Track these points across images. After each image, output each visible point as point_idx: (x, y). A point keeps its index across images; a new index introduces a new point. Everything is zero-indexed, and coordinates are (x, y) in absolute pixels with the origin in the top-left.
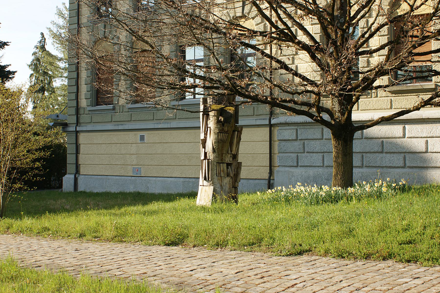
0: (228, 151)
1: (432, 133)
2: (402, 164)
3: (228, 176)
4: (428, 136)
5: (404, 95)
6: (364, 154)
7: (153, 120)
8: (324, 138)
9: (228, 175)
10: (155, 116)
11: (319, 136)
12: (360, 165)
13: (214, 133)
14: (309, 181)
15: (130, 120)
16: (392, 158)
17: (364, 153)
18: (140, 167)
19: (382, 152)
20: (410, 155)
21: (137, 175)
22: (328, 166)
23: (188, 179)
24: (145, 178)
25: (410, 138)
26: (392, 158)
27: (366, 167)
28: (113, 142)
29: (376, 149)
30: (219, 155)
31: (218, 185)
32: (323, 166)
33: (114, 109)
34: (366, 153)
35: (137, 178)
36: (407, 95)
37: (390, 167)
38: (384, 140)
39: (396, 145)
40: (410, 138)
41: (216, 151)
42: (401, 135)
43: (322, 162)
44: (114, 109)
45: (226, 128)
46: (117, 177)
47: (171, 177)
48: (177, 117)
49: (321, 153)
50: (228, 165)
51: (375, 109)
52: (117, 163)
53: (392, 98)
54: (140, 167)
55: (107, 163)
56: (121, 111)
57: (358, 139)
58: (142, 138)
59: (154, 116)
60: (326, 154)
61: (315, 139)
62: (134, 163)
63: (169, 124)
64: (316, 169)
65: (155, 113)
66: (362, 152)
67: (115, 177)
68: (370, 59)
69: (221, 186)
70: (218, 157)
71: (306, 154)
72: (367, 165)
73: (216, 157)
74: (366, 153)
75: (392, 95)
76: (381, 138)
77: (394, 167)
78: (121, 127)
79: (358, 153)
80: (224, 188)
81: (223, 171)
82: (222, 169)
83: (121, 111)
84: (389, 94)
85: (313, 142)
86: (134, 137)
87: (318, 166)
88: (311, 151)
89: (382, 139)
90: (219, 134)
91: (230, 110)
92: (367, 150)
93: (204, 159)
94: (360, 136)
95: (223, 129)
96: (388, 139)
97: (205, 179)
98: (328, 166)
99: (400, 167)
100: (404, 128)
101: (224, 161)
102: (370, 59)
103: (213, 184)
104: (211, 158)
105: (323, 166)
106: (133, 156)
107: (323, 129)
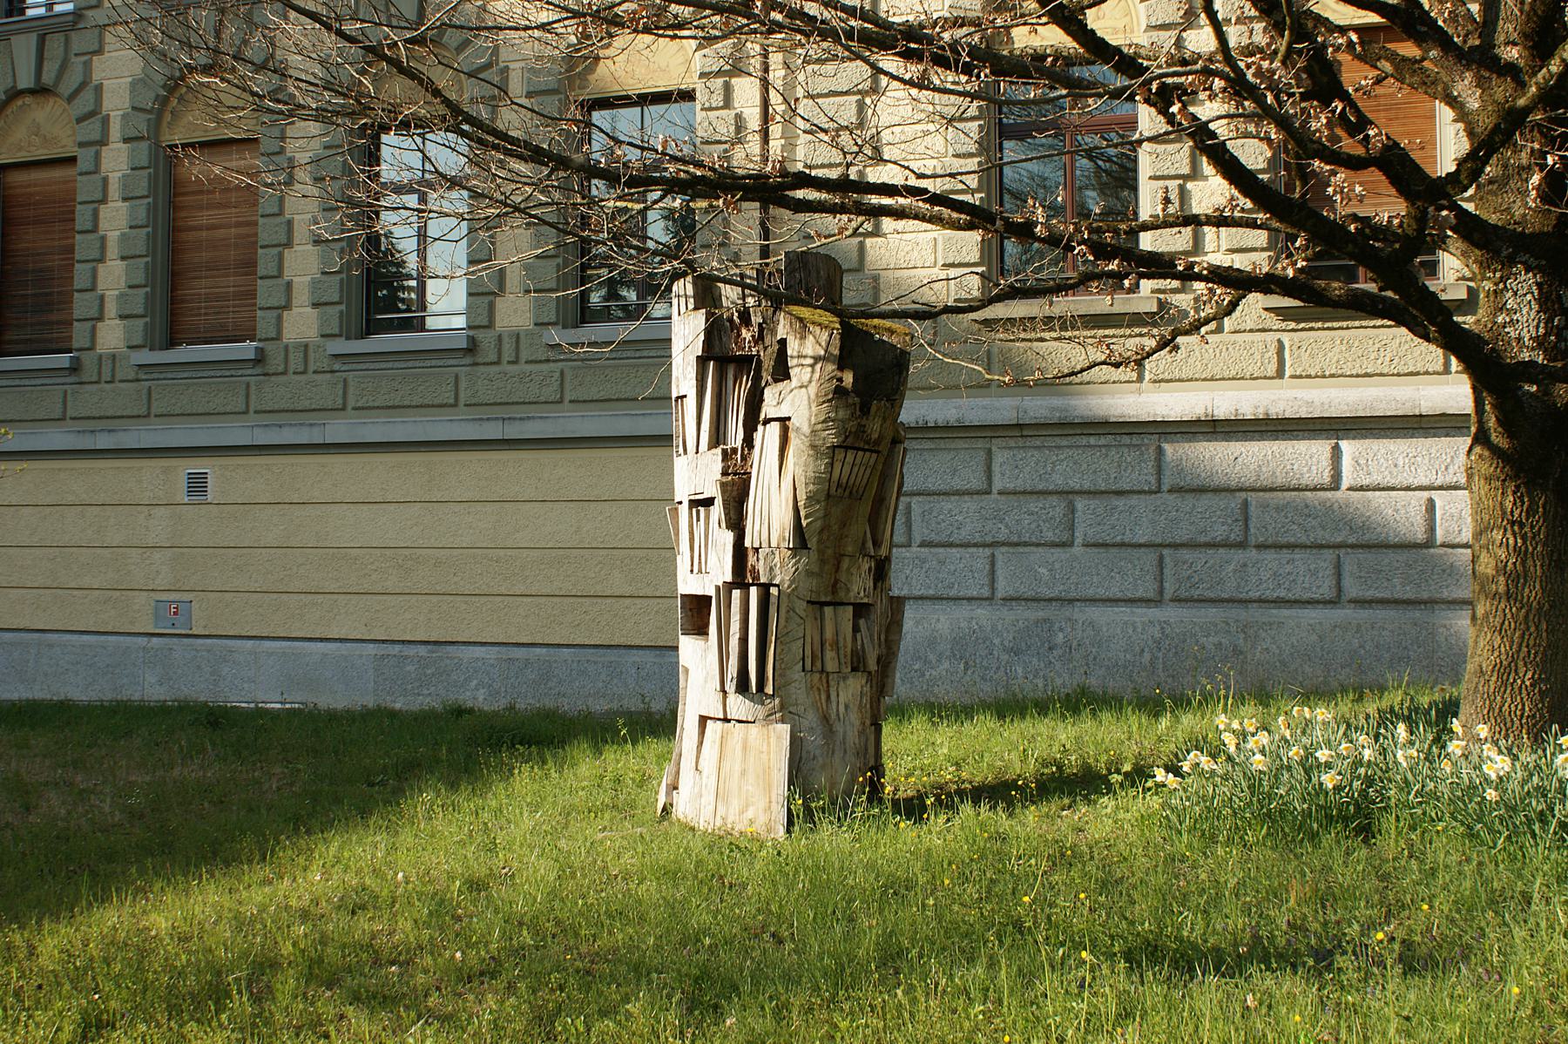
0: (864, 543)
1: (1451, 470)
2: (1326, 589)
3: (854, 669)
4: (1438, 483)
5: (1335, 324)
6: (1166, 552)
7: (246, 412)
8: (998, 484)
9: (858, 665)
10: (253, 397)
11: (976, 483)
12: (1151, 595)
13: (813, 447)
14: (932, 657)
15: (143, 411)
16: (1289, 568)
17: (1169, 546)
18: (186, 597)
19: (1242, 545)
20: (1362, 555)
21: (174, 626)
22: (1012, 599)
23: (398, 647)
24: (209, 641)
25: (1361, 489)
26: (1289, 568)
27: (1177, 600)
28: (70, 499)
29: (1219, 532)
30: (822, 561)
31: (811, 719)
32: (990, 599)
33: (75, 368)
34: (1175, 546)
35: (175, 640)
36: (1345, 324)
37: (1279, 602)
38: (1252, 496)
39: (1307, 511)
40: (1361, 489)
41: (813, 543)
42: (1326, 478)
43: (986, 581)
44: (75, 368)
45: (877, 427)
46: (85, 637)
47: (321, 640)
48: (351, 403)
49: (984, 545)
50: (861, 610)
51: (1212, 379)
52: (86, 581)
53: (1286, 339)
54: (186, 597)
55: (39, 582)
56: (106, 375)
57: (1144, 492)
58: (197, 484)
59: (247, 396)
60: (1004, 549)
61: (958, 493)
62: (160, 582)
63: (316, 430)
64: (962, 612)
65: (253, 388)
66: (1160, 545)
67: (75, 637)
68: (1189, 185)
69: (825, 719)
70: (819, 575)
71: (914, 549)
72: (1184, 595)
73: (809, 573)
74: (1175, 546)
75: (1283, 325)
76: (1241, 490)
77: (1296, 602)
78: (104, 442)
79: (1141, 546)
80: (839, 728)
81: (836, 645)
82: (829, 634)
83: (106, 375)
84: (1273, 321)
85: (947, 504)
86: (150, 478)
87: (970, 599)
88: (943, 538)
89: (1243, 495)
90: (840, 455)
91: (891, 332)
92: (1182, 535)
93: (729, 587)
94: (1153, 480)
95: (861, 429)
96: (1267, 495)
97: (743, 687)
98: (1012, 599)
99: (1318, 602)
100: (1336, 453)
101: (842, 595)
102: (1189, 185)
103: (786, 712)
104: (783, 577)
105: (990, 599)
106: (157, 555)
107: (989, 452)
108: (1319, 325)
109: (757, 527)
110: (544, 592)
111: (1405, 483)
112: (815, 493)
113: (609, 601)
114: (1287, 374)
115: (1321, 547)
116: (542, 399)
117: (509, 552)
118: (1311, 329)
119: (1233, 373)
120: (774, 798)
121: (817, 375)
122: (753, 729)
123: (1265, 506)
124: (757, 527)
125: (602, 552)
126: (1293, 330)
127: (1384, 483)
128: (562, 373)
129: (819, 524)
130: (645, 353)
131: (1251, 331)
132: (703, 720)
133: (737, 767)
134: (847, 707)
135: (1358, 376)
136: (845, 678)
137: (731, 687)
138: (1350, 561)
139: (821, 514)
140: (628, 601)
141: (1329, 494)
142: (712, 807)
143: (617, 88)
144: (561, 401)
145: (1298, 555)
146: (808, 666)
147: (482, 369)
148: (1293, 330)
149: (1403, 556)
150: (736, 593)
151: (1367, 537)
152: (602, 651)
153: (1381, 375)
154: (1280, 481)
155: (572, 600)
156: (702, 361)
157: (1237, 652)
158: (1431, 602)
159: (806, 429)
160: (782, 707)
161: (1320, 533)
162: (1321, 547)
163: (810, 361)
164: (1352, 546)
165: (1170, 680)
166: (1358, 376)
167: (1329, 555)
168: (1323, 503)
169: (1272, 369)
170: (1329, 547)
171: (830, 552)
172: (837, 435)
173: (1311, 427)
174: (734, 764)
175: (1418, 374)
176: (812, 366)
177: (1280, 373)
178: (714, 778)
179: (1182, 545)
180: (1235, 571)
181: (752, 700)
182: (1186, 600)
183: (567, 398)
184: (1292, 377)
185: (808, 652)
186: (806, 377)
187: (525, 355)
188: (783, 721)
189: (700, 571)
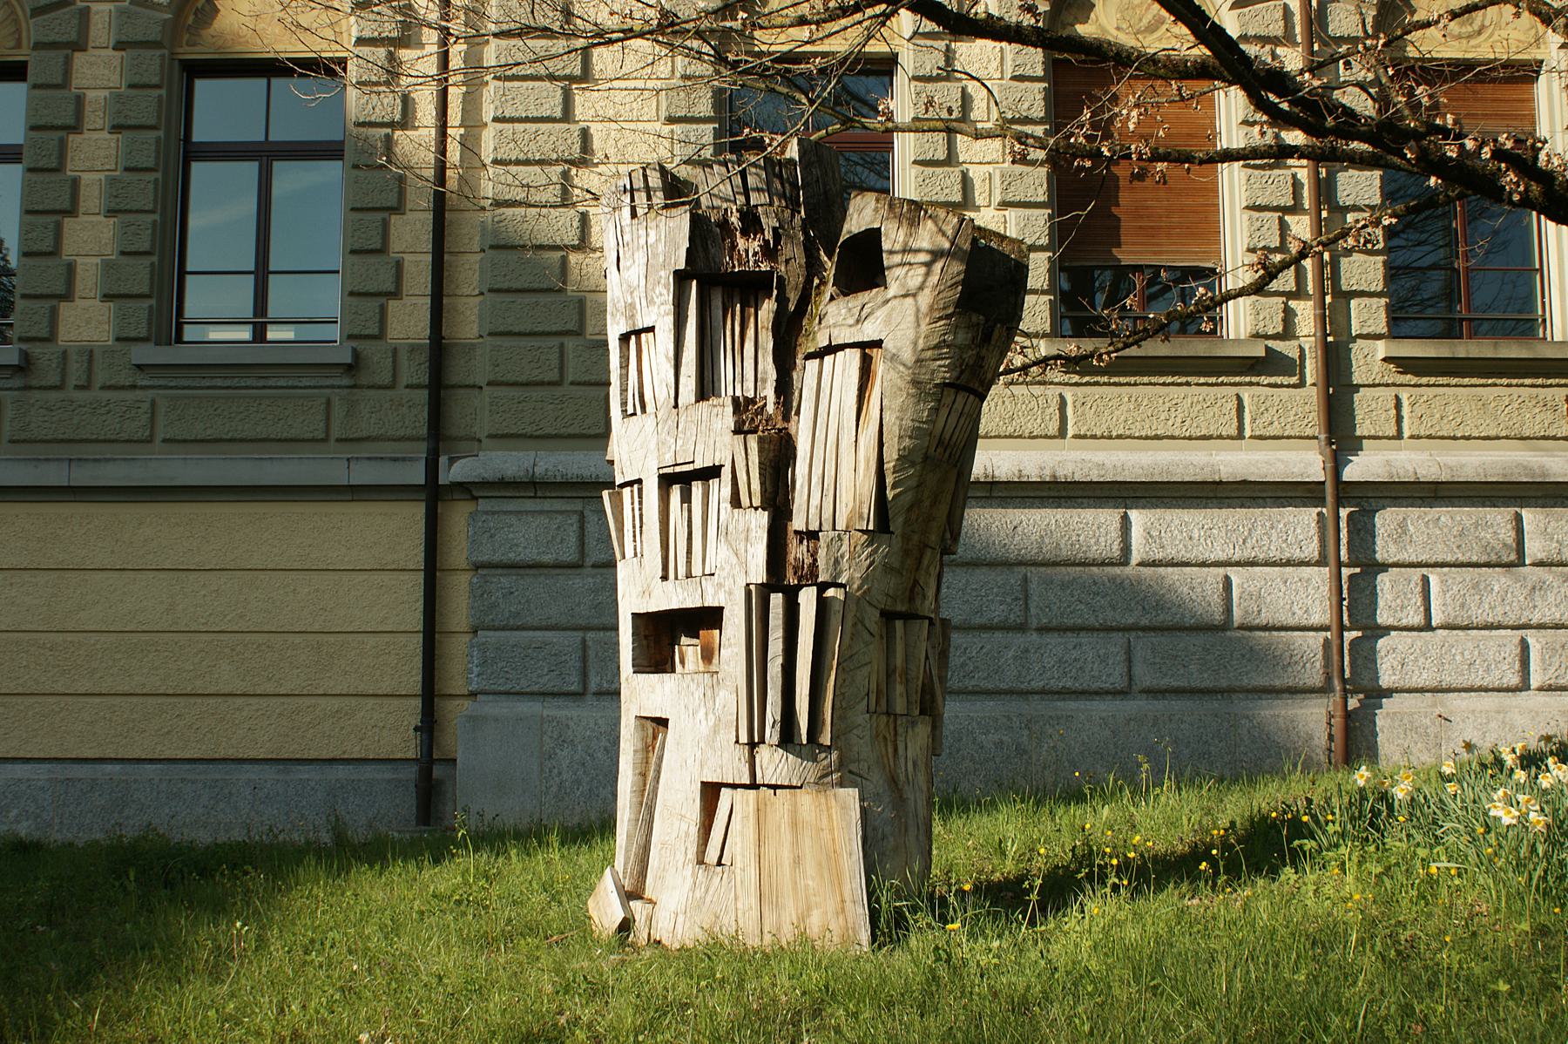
1: (1249, 545)
4: (1236, 558)
5: (1123, 380)
13: (915, 383)
16: (1075, 654)
19: (1021, 628)
20: (1154, 638)
26: (1075, 654)
29: (997, 613)
30: (906, 553)
31: (877, 780)
36: (1132, 380)
40: (1154, 564)
41: (897, 524)
42: (1116, 550)
53: (1069, 394)
69: (893, 781)
73: (887, 568)
75: (1066, 378)
76: (1021, 563)
77: (1083, 692)
89: (1023, 569)
93: (766, 590)
96: (1049, 570)
99: (1107, 693)
100: (1126, 524)
103: (847, 774)
108: (1105, 379)
109: (815, 501)
110: (120, 689)
111: (1201, 558)
112: (911, 451)
113: (212, 701)
114: (1070, 433)
115: (1111, 629)
116: (124, 436)
117: (70, 637)
118: (1097, 384)
119: (1010, 430)
120: (847, 897)
121: (934, 279)
122: (806, 799)
123: (1049, 582)
124: (815, 501)
125: (205, 637)
126: (1076, 384)
127: (1179, 557)
128: (153, 404)
129: (909, 496)
130: (271, 382)
132: (711, 792)
133: (786, 855)
134: (915, 764)
135: (1147, 438)
136: (914, 724)
137: (772, 734)
138: (1143, 646)
139: (913, 483)
140: (240, 701)
141: (1117, 570)
142: (755, 914)
143: (238, 48)
144: (150, 440)
145: (1084, 638)
146: (872, 708)
147: (37, 394)
148: (1076, 384)
149: (1200, 639)
150: (777, 600)
151: (1161, 618)
152: (201, 767)
153: (1173, 437)
154: (1065, 553)
155: (160, 700)
156: (681, 278)
157: (1021, 751)
158: (1230, 691)
159: (908, 356)
160: (842, 764)
161: (1110, 613)
162: (1111, 629)
164: (1145, 629)
166: (1147, 438)
167: (1118, 637)
168: (1112, 579)
169: (1053, 427)
170: (1118, 629)
171: (916, 538)
172: (950, 368)
173: (1098, 493)
174: (781, 849)
175: (1210, 437)
177: (1062, 433)
178: (752, 872)
180: (1015, 658)
181: (799, 755)
183: (160, 436)
184: (1075, 437)
185: (873, 686)
187: (100, 377)
188: (841, 784)
189: (689, 576)
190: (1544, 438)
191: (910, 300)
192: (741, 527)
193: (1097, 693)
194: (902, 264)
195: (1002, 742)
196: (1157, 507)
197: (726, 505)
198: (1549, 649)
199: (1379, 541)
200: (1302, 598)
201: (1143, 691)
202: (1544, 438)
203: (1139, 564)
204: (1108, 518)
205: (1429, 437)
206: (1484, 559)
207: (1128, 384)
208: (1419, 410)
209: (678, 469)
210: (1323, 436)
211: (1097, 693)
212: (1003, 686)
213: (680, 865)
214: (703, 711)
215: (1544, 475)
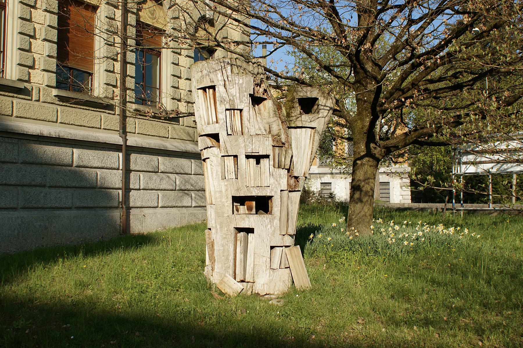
53: (59, 108)
76: (46, 164)
77: (61, 208)
126: (61, 105)
131: (49, 103)
141: (70, 168)
148: (61, 105)
153: (85, 126)
154: (58, 161)
163: (328, 108)
165: (24, 241)
176: (329, 110)
179: (26, 185)
182: (28, 208)
186: (325, 114)
190: (164, 137)
191: (323, 119)
192: (277, 173)
193: (64, 208)
194: (323, 109)
195: (41, 225)
196: (80, 148)
197: (272, 167)
198: (163, 196)
199: (131, 164)
200: (115, 179)
201: (76, 208)
202: (164, 137)
203: (76, 167)
204: (68, 150)
205: (141, 134)
206: (152, 170)
207: (74, 107)
208: (140, 126)
209: (253, 154)
210: (121, 131)
211: (64, 208)
212: (40, 206)
213: (264, 270)
214: (269, 226)
215: (167, 148)
